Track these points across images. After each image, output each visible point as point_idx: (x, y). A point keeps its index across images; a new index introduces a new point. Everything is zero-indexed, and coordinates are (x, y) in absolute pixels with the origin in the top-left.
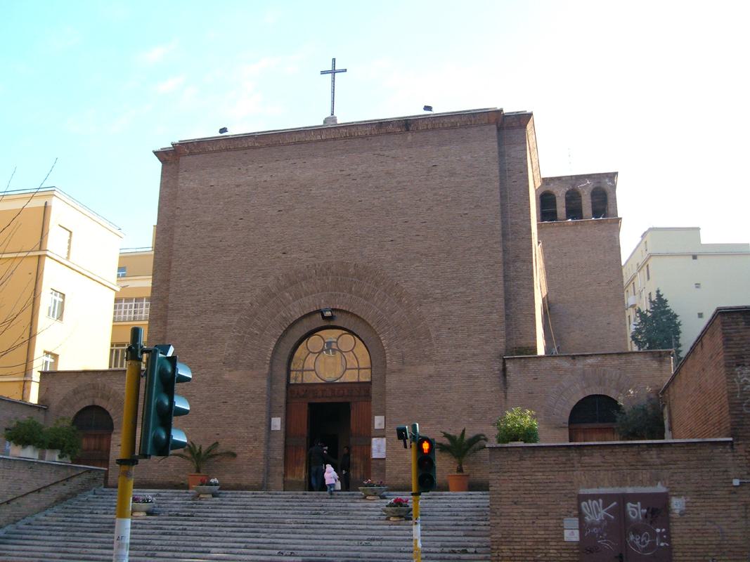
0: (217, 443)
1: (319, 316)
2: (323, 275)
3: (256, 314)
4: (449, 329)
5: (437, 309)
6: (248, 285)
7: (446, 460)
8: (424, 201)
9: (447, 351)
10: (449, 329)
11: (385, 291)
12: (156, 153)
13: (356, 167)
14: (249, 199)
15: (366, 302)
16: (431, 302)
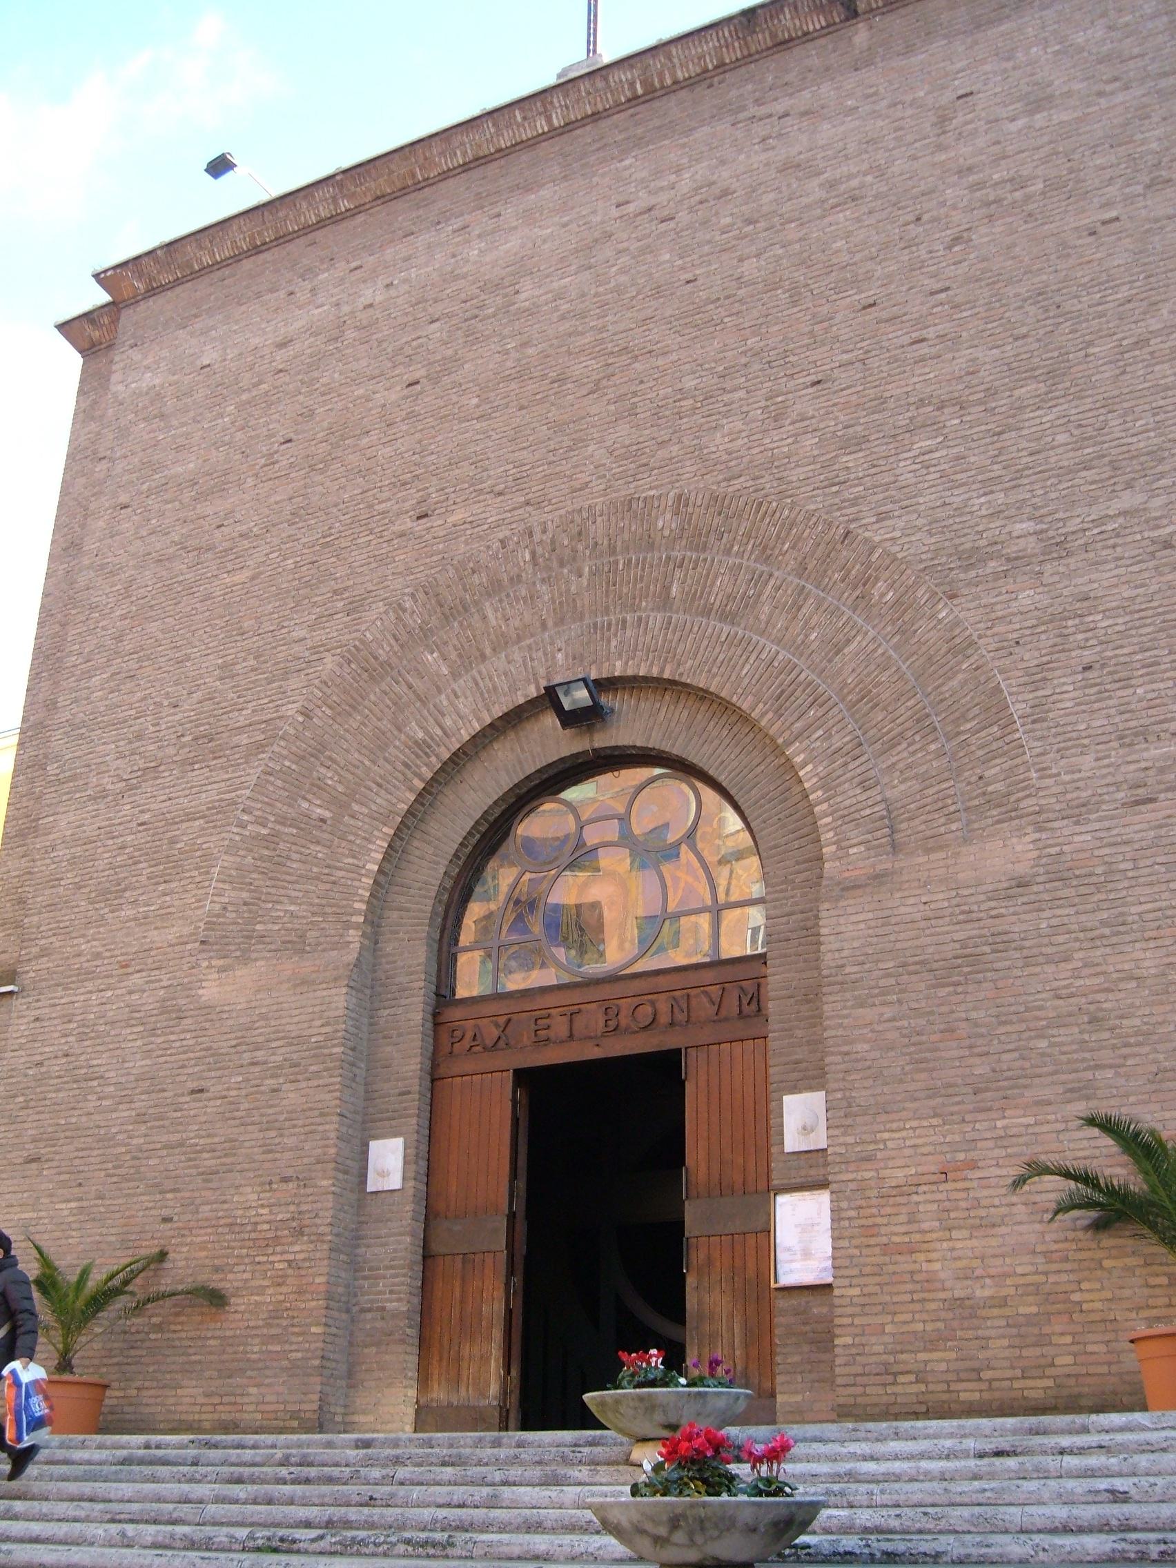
0: (162, 1256)
1: (550, 721)
2: (562, 565)
3: (323, 747)
4: (1087, 668)
5: (1027, 598)
6: (297, 649)
7: (1130, 1270)
8: (935, 220)
9: (1088, 761)
10: (1087, 668)
11: (801, 570)
12: (64, 328)
13: (673, 178)
14: (315, 374)
15: (726, 629)
16: (997, 576)
